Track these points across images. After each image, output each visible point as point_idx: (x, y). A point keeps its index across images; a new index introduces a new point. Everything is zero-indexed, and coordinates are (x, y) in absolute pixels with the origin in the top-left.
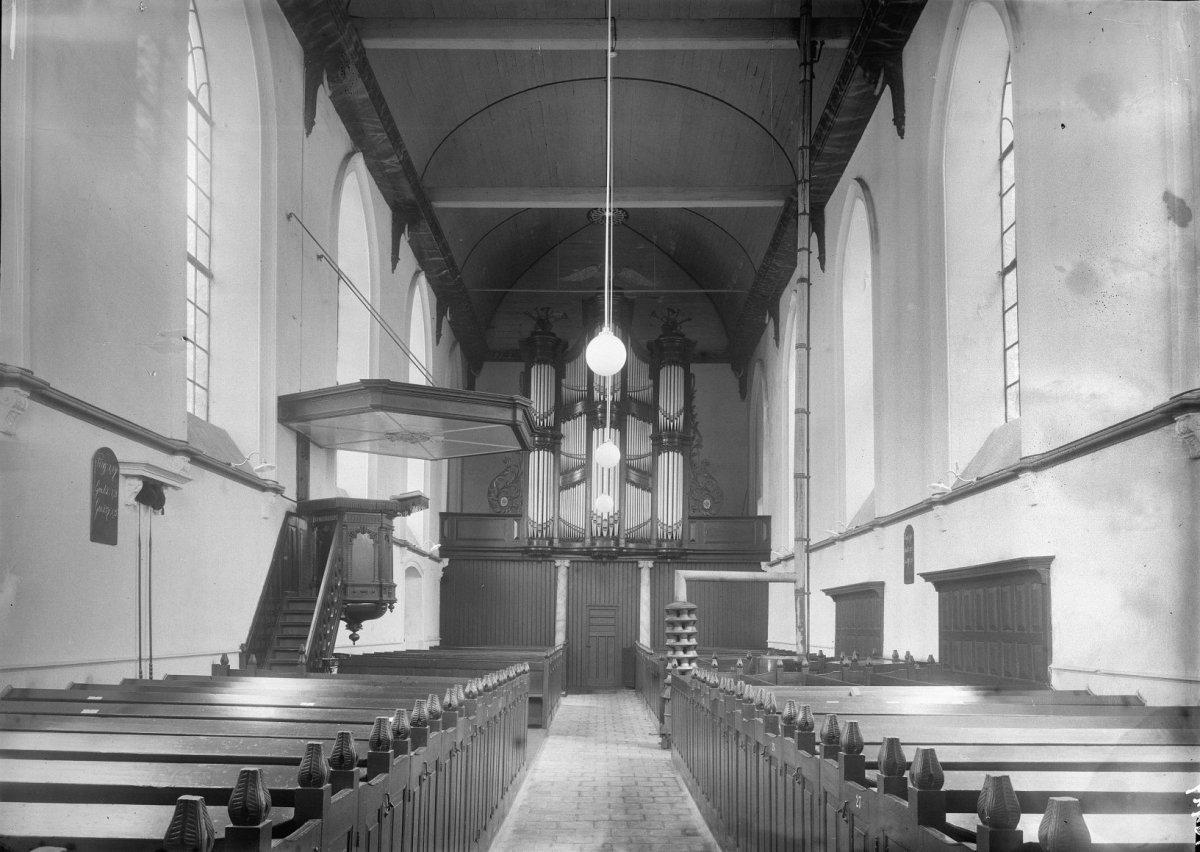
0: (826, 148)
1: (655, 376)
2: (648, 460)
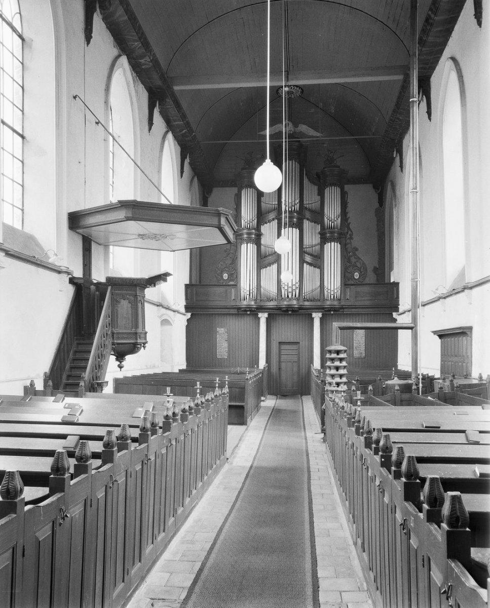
0: (429, 38)
1: (321, 194)
2: (318, 248)
